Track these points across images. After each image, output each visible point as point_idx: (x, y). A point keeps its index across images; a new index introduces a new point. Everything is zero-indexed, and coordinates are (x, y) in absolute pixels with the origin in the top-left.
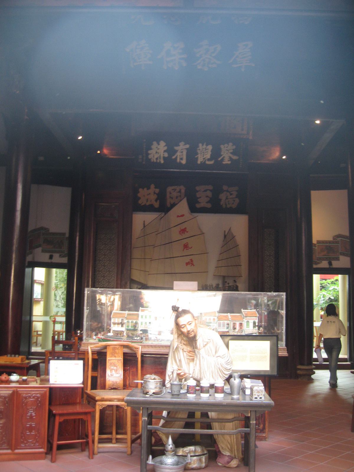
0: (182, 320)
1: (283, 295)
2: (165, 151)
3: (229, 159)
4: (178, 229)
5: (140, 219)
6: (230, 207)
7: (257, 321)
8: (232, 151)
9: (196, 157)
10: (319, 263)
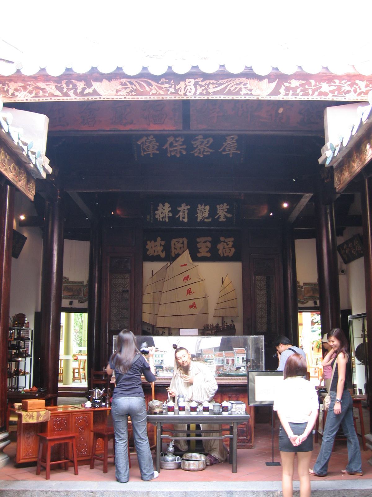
0: (179, 354)
1: (262, 337)
2: (169, 212)
3: (224, 217)
4: (182, 276)
5: (150, 268)
6: (227, 256)
7: (245, 357)
8: (226, 210)
9: (196, 216)
10: (305, 303)
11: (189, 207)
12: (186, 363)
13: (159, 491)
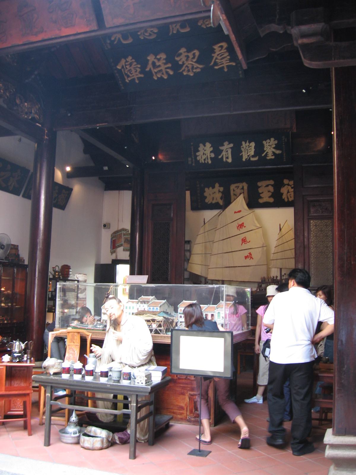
2: (211, 152)
8: (274, 146)
9: (241, 155)
11: (232, 145)
12: (113, 316)
13: (5, 471)
